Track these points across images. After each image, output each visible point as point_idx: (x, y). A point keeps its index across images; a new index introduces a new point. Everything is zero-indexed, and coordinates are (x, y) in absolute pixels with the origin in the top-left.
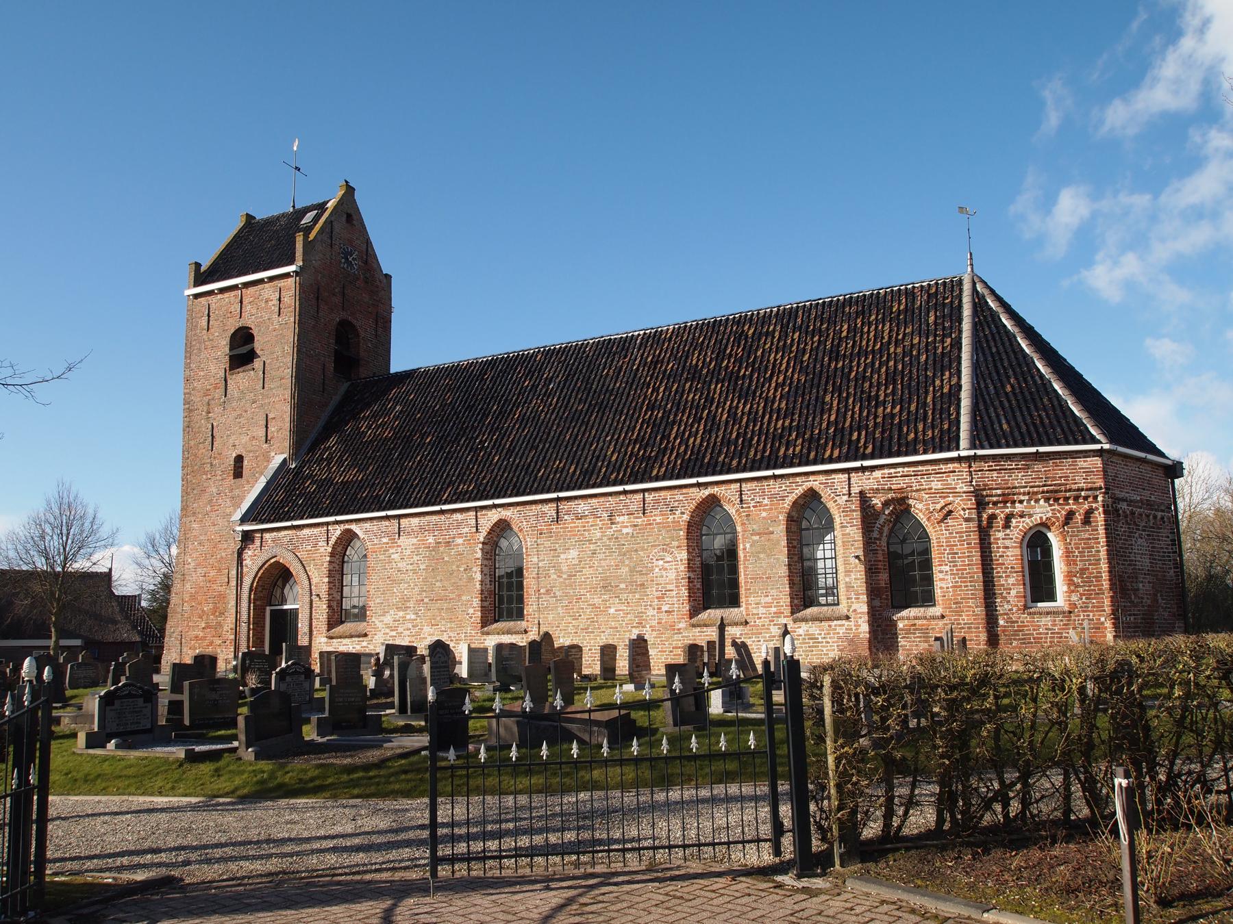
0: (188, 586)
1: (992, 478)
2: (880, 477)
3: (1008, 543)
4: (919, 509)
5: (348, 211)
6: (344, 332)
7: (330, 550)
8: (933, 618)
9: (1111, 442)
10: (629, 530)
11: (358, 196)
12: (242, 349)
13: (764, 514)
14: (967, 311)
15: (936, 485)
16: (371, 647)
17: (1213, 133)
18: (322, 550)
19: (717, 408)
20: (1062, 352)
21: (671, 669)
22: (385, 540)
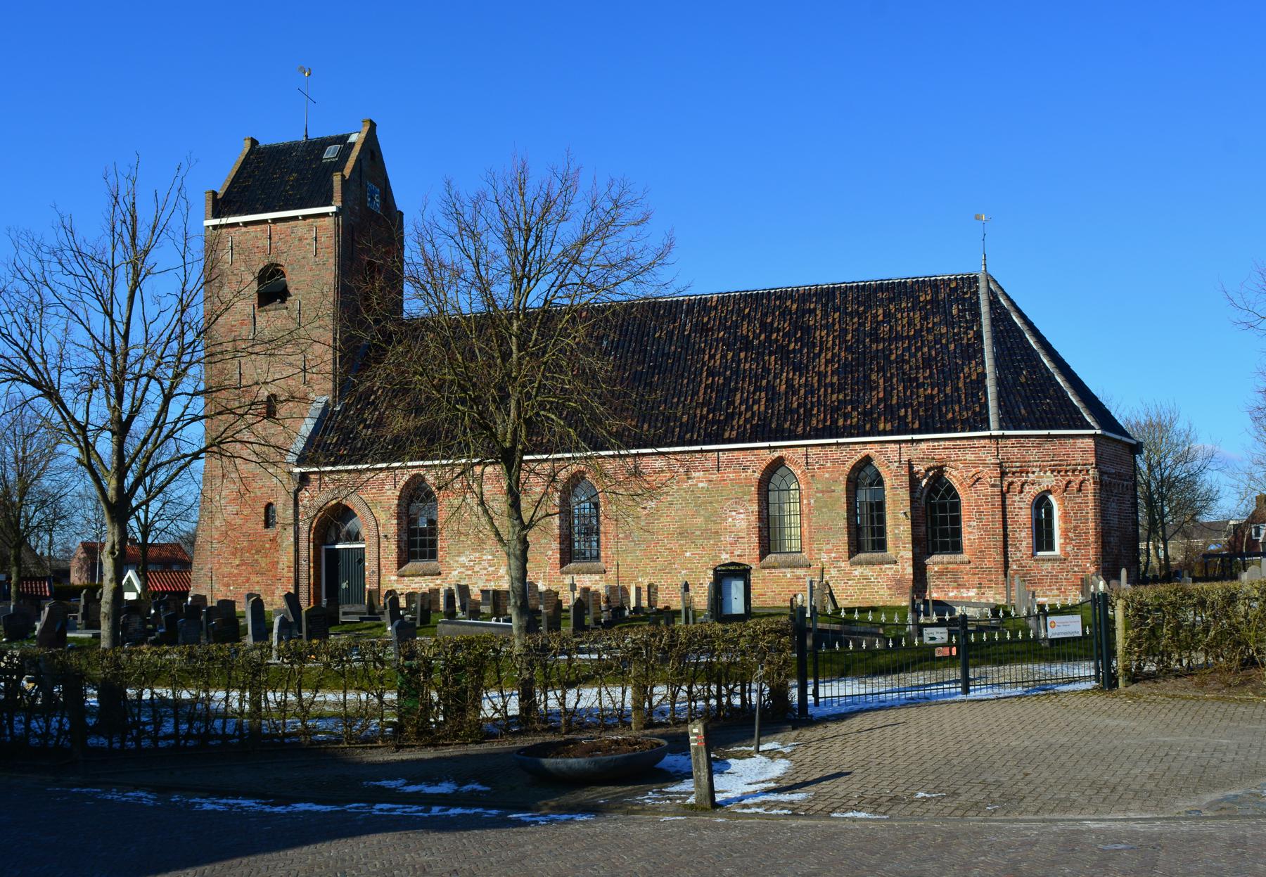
0: (217, 523)
1: (1012, 452)
2: (925, 449)
3: (1022, 505)
4: (954, 476)
5: (371, 146)
8: (962, 563)
9: (1102, 428)
12: (272, 288)
13: (827, 475)
14: (984, 308)
15: (970, 457)
19: (775, 378)
20: (1048, 339)
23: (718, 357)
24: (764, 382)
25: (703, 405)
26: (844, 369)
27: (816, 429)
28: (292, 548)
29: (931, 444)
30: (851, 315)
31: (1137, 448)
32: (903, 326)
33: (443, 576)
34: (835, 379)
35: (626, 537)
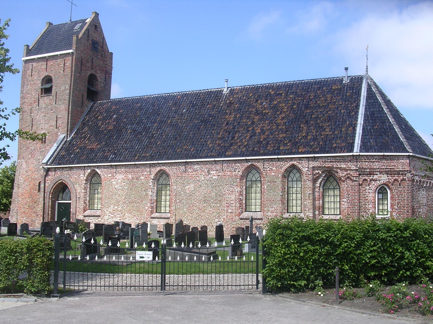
5: (96, 25)
6: (92, 79)
7: (85, 178)
9: (414, 151)
10: (216, 177)
11: (100, 17)
13: (273, 174)
16: (103, 221)
17: (15, 237)
18: (82, 178)
21: (232, 237)
22: (110, 175)
28: (42, 202)
35: (180, 202)
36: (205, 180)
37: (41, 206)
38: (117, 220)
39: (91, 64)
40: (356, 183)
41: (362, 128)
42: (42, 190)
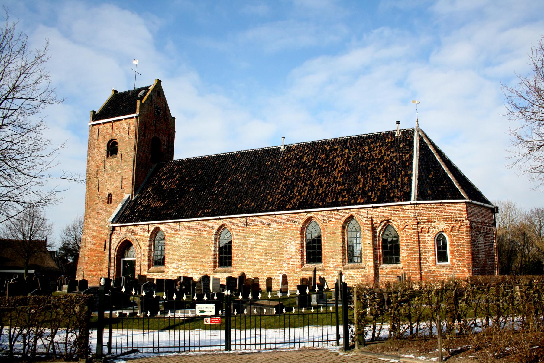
2: (378, 212)
3: (429, 239)
5: (158, 89)
7: (149, 235)
8: (399, 268)
11: (162, 84)
12: (112, 149)
13: (332, 225)
15: (401, 215)
18: (146, 235)
19: (314, 180)
22: (173, 232)
23: (291, 171)
24: (309, 182)
25: (280, 193)
26: (346, 174)
27: (328, 203)
28: (108, 260)
29: (382, 208)
30: (353, 150)
31: (495, 210)
32: (376, 154)
33: (166, 272)
34: (341, 180)
35: (242, 255)
36: (266, 234)
37: (106, 264)
38: (179, 275)
39: (154, 127)
40: (415, 231)
41: (417, 178)
42: (108, 248)
